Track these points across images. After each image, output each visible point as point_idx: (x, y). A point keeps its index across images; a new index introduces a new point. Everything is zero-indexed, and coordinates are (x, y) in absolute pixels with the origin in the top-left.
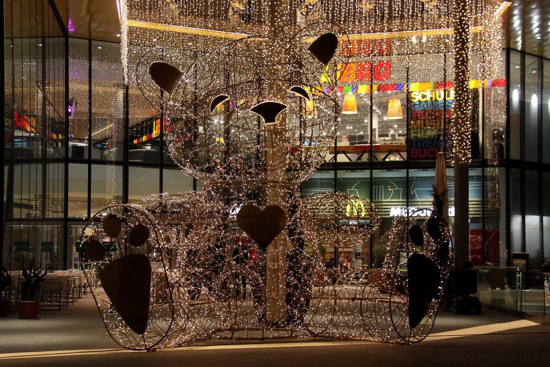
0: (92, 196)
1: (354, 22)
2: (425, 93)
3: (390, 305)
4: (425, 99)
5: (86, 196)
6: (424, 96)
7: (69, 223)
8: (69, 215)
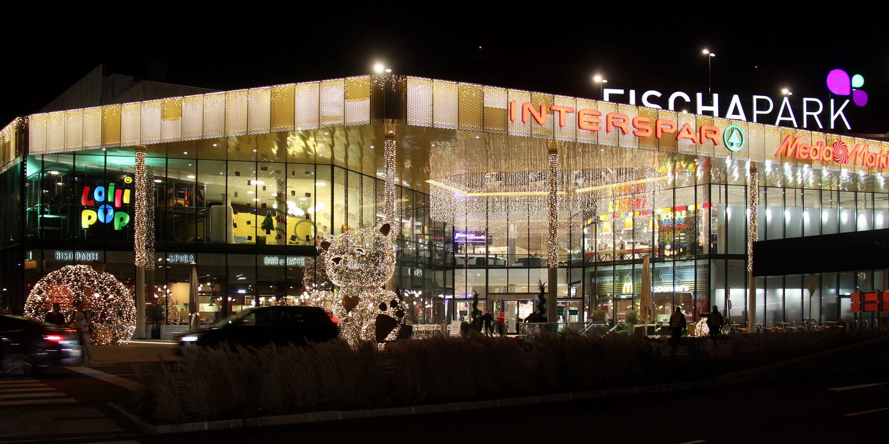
0: (489, 284)
1: (499, 140)
2: (668, 215)
3: (831, 193)
4: (668, 218)
5: (485, 284)
6: (667, 216)
7: (455, 301)
8: (740, 253)
